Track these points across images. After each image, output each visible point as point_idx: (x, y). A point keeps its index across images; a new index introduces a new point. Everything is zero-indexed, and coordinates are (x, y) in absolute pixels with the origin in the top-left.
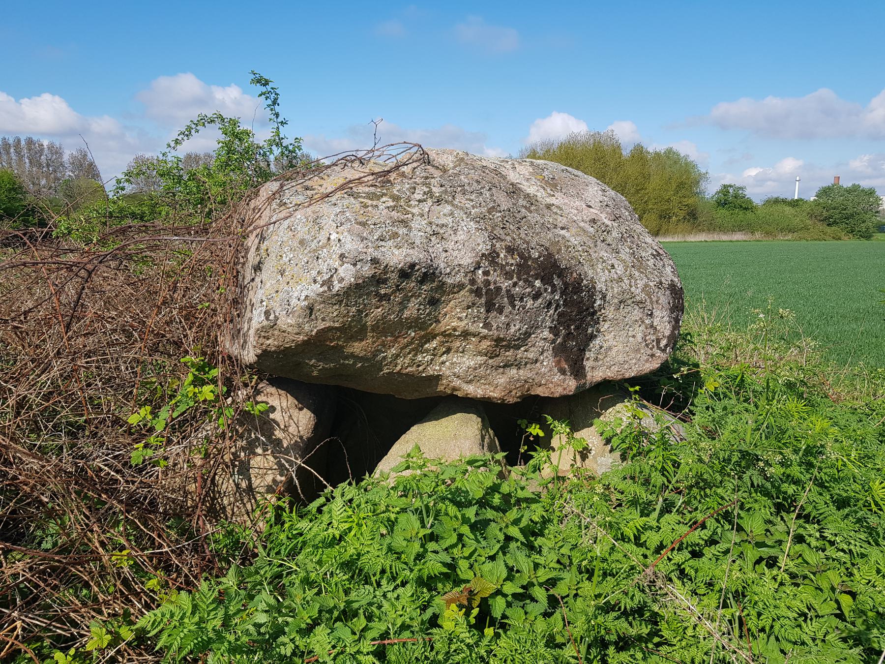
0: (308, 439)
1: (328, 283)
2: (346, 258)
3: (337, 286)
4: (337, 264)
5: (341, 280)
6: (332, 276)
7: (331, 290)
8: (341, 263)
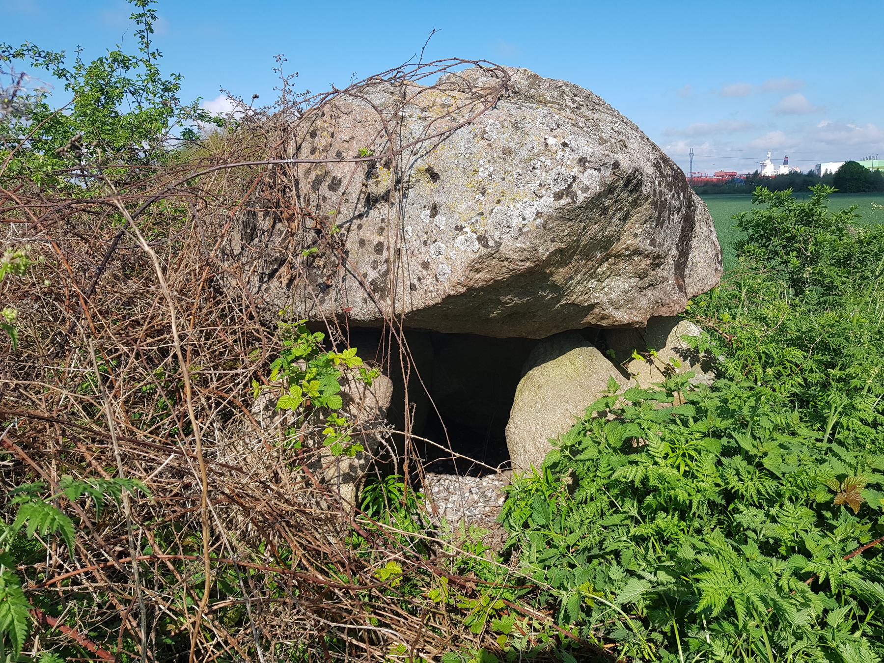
0: (388, 409)
1: (568, 191)
2: (589, 162)
3: (581, 197)
4: (575, 171)
5: (586, 189)
6: (570, 186)
7: (575, 202)
8: (581, 169)
